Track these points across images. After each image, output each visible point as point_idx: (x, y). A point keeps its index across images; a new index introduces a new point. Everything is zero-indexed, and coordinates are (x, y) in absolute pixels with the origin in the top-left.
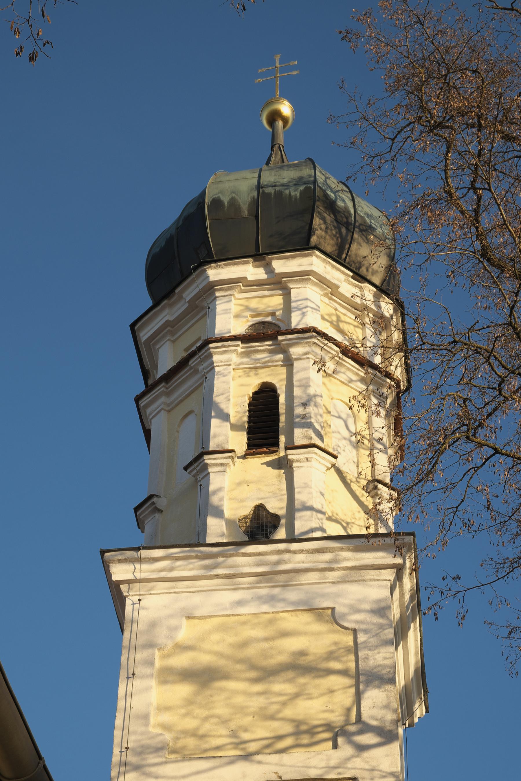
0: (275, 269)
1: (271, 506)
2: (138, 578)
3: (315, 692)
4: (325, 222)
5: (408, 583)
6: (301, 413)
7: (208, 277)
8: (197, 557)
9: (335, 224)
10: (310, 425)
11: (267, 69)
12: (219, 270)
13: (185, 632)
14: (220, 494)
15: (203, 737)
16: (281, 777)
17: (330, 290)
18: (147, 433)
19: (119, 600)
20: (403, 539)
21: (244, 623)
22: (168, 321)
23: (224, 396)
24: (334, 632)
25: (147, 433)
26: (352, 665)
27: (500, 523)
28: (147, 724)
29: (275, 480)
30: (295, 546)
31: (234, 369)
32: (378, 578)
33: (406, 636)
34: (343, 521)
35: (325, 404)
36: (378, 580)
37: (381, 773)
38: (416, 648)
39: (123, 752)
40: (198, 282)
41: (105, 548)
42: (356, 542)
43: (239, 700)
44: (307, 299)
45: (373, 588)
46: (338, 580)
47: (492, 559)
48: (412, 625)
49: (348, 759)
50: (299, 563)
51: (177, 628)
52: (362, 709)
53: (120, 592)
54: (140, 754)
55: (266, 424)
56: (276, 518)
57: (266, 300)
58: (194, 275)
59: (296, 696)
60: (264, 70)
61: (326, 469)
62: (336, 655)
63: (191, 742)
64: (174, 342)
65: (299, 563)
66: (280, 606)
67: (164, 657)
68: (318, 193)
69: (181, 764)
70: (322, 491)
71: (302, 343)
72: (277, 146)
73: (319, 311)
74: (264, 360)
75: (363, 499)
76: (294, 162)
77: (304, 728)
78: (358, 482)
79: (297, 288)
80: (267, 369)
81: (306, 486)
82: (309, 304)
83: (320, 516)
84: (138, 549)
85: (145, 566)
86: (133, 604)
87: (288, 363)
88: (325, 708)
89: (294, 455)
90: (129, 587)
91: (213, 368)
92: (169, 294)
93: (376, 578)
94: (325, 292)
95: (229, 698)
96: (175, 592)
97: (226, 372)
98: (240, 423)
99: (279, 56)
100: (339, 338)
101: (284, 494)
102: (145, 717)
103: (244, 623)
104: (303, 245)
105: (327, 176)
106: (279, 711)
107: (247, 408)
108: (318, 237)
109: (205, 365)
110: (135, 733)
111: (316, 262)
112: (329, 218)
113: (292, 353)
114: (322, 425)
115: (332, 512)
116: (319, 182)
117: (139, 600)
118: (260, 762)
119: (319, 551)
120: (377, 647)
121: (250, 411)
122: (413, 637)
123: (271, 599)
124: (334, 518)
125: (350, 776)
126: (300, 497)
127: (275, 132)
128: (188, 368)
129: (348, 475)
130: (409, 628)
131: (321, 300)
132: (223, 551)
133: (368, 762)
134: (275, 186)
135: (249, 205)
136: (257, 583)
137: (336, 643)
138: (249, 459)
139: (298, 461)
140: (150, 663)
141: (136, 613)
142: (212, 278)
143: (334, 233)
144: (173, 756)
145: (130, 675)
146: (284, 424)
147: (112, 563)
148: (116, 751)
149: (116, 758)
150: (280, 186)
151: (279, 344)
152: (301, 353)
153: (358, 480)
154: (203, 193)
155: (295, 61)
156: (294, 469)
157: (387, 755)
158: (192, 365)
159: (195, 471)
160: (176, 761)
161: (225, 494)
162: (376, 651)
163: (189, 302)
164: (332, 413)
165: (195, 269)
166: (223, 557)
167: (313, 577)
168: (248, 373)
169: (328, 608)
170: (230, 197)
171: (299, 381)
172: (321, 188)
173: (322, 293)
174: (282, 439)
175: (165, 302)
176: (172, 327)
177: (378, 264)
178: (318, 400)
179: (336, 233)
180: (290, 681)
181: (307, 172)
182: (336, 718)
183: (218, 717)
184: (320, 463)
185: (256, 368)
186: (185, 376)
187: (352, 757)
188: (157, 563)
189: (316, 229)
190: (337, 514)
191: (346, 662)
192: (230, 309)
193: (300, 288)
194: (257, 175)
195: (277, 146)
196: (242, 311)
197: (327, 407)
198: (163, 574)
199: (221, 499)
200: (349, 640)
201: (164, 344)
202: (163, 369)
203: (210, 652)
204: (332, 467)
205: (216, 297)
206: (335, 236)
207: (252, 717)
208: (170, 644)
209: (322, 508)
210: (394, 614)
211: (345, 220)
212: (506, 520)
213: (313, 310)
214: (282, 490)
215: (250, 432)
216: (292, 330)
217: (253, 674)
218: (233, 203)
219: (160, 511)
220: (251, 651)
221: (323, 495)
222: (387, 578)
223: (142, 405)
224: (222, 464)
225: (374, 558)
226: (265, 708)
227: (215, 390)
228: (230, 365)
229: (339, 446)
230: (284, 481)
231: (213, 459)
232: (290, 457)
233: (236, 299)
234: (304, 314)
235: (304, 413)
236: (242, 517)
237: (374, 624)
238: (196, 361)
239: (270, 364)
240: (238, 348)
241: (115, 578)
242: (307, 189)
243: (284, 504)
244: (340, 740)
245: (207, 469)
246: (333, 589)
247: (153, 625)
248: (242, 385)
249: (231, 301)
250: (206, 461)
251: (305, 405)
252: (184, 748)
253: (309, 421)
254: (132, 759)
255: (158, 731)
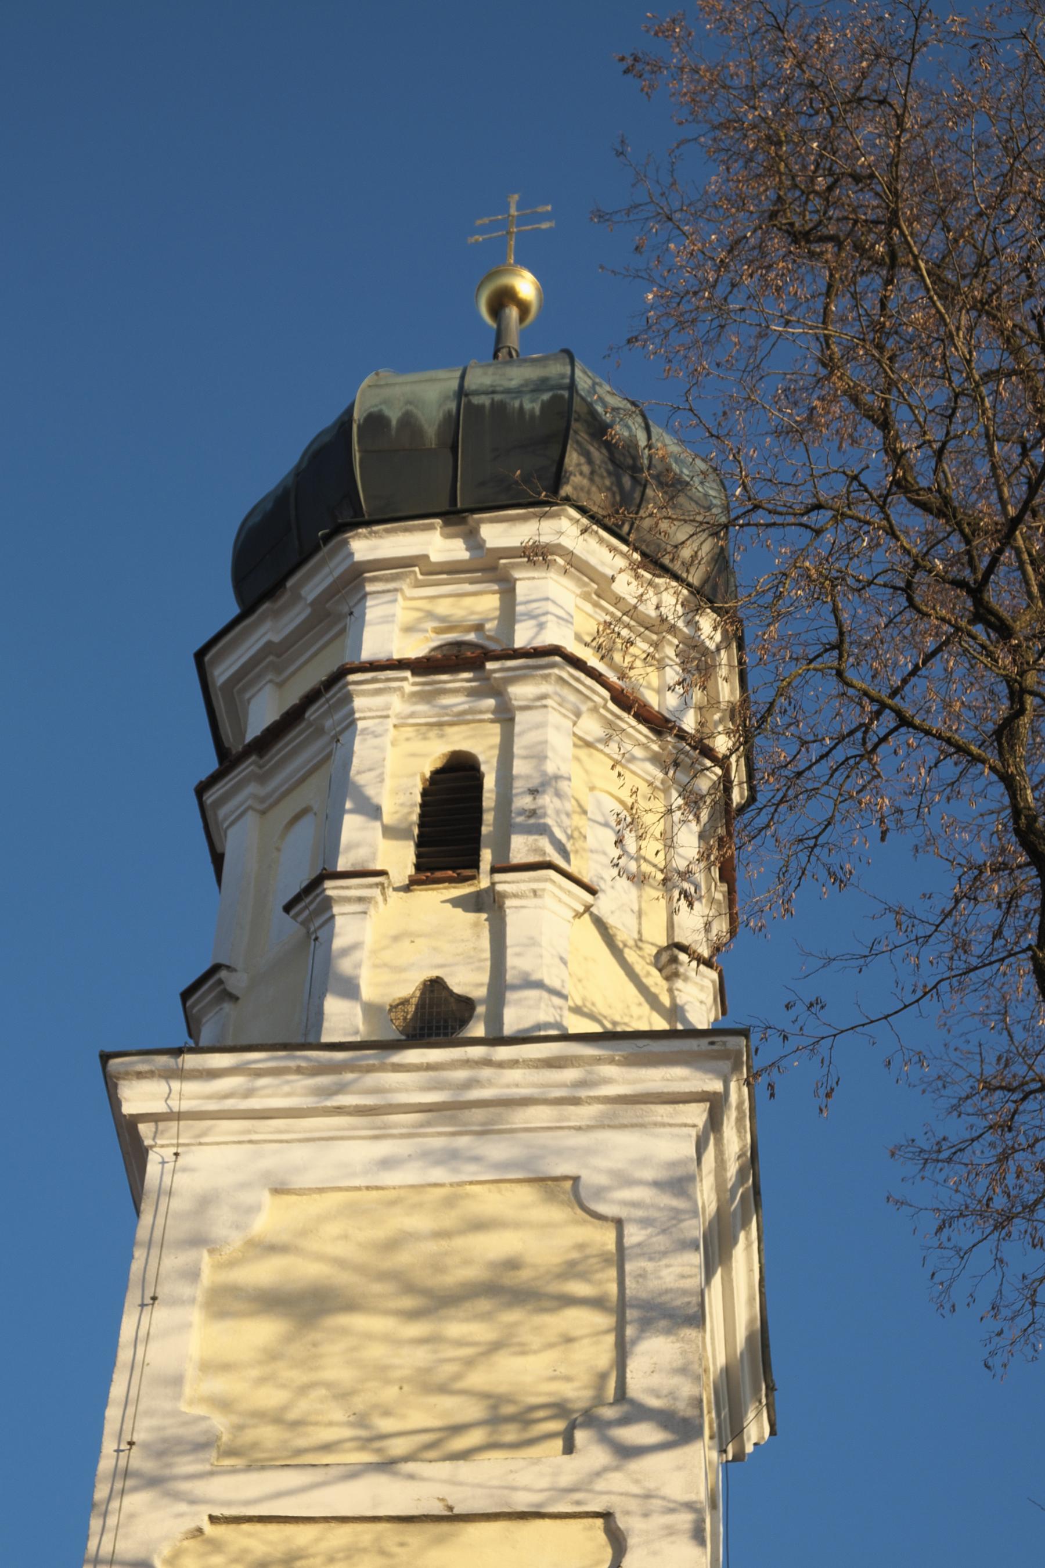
0: (484, 541)
1: (457, 981)
2: (176, 1109)
3: (535, 1341)
4: (590, 461)
5: (734, 1140)
6: (527, 807)
7: (352, 554)
8: (299, 1071)
9: (611, 467)
10: (544, 830)
11: (492, 218)
12: (373, 542)
13: (270, 1218)
14: (356, 956)
15: (296, 1424)
16: (451, 1508)
17: (595, 586)
18: (218, 860)
19: (135, 1155)
20: (724, 1043)
21: (392, 1203)
22: (269, 643)
23: (373, 774)
24: (577, 1222)
25: (218, 860)
26: (613, 1288)
27: (917, 939)
28: (178, 1397)
29: (468, 933)
30: (503, 1053)
31: (395, 726)
32: (672, 1121)
33: (730, 1257)
34: (605, 1017)
35: (577, 796)
36: (671, 1125)
37: (665, 1503)
38: (750, 1286)
39: (123, 1451)
40: (332, 564)
41: (109, 1049)
42: (629, 1046)
43: (376, 1352)
44: (547, 599)
45: (661, 1144)
46: (588, 1123)
47: (913, 1141)
48: (742, 1235)
49: (598, 1474)
50: (508, 1086)
51: (253, 1210)
52: (629, 1375)
53: (137, 1138)
54: (160, 1454)
55: (454, 825)
56: (467, 1004)
57: (468, 601)
58: (325, 550)
59: (495, 1347)
60: (486, 220)
61: (574, 914)
62: (580, 1268)
63: (268, 1434)
64: (280, 685)
65: (508, 1086)
66: (469, 1171)
67: (219, 1266)
68: (577, 405)
69: (242, 1478)
70: (564, 956)
71: (533, 676)
72: (505, 351)
73: (572, 623)
74: (456, 709)
75: (648, 981)
76: (535, 356)
77: (508, 1410)
78: (640, 949)
79: (529, 579)
80: (463, 728)
81: (533, 942)
82: (551, 607)
83: (557, 1001)
84: (178, 1052)
85: (191, 1087)
86: (163, 1163)
87: (505, 716)
88: (551, 1373)
89: (508, 883)
90: (157, 1128)
91: (353, 723)
92: (273, 590)
93: (666, 1120)
94: (586, 589)
95: (354, 1349)
96: (251, 1142)
97: (379, 730)
98: (404, 825)
99: (516, 197)
100: (612, 677)
101: (486, 960)
102: (176, 1381)
103: (392, 1203)
104: (542, 492)
105: (597, 380)
106: (458, 1377)
107: (419, 799)
108: (575, 488)
109: (337, 716)
110: (150, 1413)
111: (564, 529)
112: (597, 455)
113: (513, 697)
114: (569, 832)
115: (584, 999)
116: (579, 387)
117: (176, 1154)
118: (411, 1477)
119: (551, 1063)
120: (665, 1254)
121: (423, 806)
122: (745, 1258)
123: (451, 1157)
124: (585, 1010)
125: (598, 1510)
126: (516, 962)
127: (503, 327)
128: (303, 725)
129: (618, 933)
130: (735, 1241)
131: (577, 606)
132: (352, 1059)
133: (637, 1481)
134: (493, 392)
135: (439, 426)
136: (422, 1126)
137: (581, 1247)
138: (418, 893)
139: (515, 896)
140: (193, 1275)
141: (167, 1180)
142: (358, 557)
143: (607, 483)
144: (228, 1462)
145: (148, 1301)
146: (491, 829)
147: (124, 1079)
148: (109, 1446)
149: (106, 1464)
150: (502, 392)
151: (488, 679)
152: (531, 696)
153: (640, 944)
154: (350, 410)
155: (547, 205)
156: (508, 911)
157: (679, 1468)
158: (312, 718)
159: (307, 912)
160: (233, 1471)
161: (362, 955)
162: (664, 1262)
163: (312, 604)
164: (589, 815)
165: (327, 539)
166: (352, 1071)
167: (539, 1115)
168: (424, 734)
169: (566, 1178)
170: (403, 410)
171: (526, 747)
172: (583, 399)
173: (578, 591)
174: (486, 856)
175: (266, 606)
176: (279, 656)
177: (695, 549)
178: (563, 785)
179: (612, 484)
180: (485, 1317)
181: (557, 369)
182: (576, 1393)
183: (328, 1385)
184: (560, 900)
185: (440, 725)
186: (297, 741)
187: (605, 1470)
188: (219, 1080)
189: (571, 474)
190: (593, 1004)
191: (600, 1283)
192: (394, 615)
193: (534, 578)
194: (458, 374)
195: (505, 351)
196: (419, 620)
197: (583, 803)
198: (230, 1104)
199: (358, 965)
200: (607, 1238)
201: (260, 690)
202: (254, 729)
203: (320, 1257)
204: (585, 912)
205: (365, 596)
206: (609, 489)
207: (396, 1388)
208: (237, 1240)
209: (563, 986)
210: (703, 1203)
211: (630, 461)
212: (928, 933)
213: (561, 622)
214: (482, 951)
215: (421, 844)
216: (515, 650)
217: (408, 1302)
218: (408, 422)
219: (234, 998)
220: (404, 1258)
221: (565, 963)
222: (689, 1121)
223: (209, 802)
224: (360, 900)
225: (664, 1079)
226: (428, 1370)
227: (356, 761)
228: (387, 717)
229: (602, 878)
230: (486, 934)
231: (342, 888)
232: (499, 888)
233: (406, 598)
234: (541, 626)
235: (532, 807)
236: (397, 1002)
237: (660, 1209)
238: (319, 714)
239: (469, 717)
240: (405, 684)
241: (128, 1108)
242: (555, 399)
243: (485, 978)
244: (581, 1436)
245: (330, 908)
246: (581, 1140)
247: (205, 1202)
248: (413, 755)
249: (395, 601)
250: (329, 893)
251: (534, 792)
252: (255, 1446)
253: (542, 821)
254: (137, 1461)
255: (200, 1411)
